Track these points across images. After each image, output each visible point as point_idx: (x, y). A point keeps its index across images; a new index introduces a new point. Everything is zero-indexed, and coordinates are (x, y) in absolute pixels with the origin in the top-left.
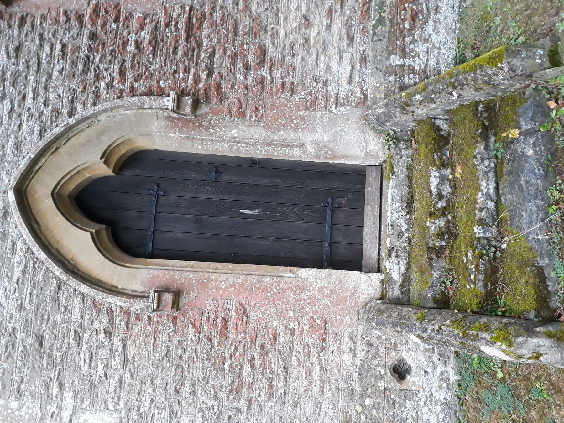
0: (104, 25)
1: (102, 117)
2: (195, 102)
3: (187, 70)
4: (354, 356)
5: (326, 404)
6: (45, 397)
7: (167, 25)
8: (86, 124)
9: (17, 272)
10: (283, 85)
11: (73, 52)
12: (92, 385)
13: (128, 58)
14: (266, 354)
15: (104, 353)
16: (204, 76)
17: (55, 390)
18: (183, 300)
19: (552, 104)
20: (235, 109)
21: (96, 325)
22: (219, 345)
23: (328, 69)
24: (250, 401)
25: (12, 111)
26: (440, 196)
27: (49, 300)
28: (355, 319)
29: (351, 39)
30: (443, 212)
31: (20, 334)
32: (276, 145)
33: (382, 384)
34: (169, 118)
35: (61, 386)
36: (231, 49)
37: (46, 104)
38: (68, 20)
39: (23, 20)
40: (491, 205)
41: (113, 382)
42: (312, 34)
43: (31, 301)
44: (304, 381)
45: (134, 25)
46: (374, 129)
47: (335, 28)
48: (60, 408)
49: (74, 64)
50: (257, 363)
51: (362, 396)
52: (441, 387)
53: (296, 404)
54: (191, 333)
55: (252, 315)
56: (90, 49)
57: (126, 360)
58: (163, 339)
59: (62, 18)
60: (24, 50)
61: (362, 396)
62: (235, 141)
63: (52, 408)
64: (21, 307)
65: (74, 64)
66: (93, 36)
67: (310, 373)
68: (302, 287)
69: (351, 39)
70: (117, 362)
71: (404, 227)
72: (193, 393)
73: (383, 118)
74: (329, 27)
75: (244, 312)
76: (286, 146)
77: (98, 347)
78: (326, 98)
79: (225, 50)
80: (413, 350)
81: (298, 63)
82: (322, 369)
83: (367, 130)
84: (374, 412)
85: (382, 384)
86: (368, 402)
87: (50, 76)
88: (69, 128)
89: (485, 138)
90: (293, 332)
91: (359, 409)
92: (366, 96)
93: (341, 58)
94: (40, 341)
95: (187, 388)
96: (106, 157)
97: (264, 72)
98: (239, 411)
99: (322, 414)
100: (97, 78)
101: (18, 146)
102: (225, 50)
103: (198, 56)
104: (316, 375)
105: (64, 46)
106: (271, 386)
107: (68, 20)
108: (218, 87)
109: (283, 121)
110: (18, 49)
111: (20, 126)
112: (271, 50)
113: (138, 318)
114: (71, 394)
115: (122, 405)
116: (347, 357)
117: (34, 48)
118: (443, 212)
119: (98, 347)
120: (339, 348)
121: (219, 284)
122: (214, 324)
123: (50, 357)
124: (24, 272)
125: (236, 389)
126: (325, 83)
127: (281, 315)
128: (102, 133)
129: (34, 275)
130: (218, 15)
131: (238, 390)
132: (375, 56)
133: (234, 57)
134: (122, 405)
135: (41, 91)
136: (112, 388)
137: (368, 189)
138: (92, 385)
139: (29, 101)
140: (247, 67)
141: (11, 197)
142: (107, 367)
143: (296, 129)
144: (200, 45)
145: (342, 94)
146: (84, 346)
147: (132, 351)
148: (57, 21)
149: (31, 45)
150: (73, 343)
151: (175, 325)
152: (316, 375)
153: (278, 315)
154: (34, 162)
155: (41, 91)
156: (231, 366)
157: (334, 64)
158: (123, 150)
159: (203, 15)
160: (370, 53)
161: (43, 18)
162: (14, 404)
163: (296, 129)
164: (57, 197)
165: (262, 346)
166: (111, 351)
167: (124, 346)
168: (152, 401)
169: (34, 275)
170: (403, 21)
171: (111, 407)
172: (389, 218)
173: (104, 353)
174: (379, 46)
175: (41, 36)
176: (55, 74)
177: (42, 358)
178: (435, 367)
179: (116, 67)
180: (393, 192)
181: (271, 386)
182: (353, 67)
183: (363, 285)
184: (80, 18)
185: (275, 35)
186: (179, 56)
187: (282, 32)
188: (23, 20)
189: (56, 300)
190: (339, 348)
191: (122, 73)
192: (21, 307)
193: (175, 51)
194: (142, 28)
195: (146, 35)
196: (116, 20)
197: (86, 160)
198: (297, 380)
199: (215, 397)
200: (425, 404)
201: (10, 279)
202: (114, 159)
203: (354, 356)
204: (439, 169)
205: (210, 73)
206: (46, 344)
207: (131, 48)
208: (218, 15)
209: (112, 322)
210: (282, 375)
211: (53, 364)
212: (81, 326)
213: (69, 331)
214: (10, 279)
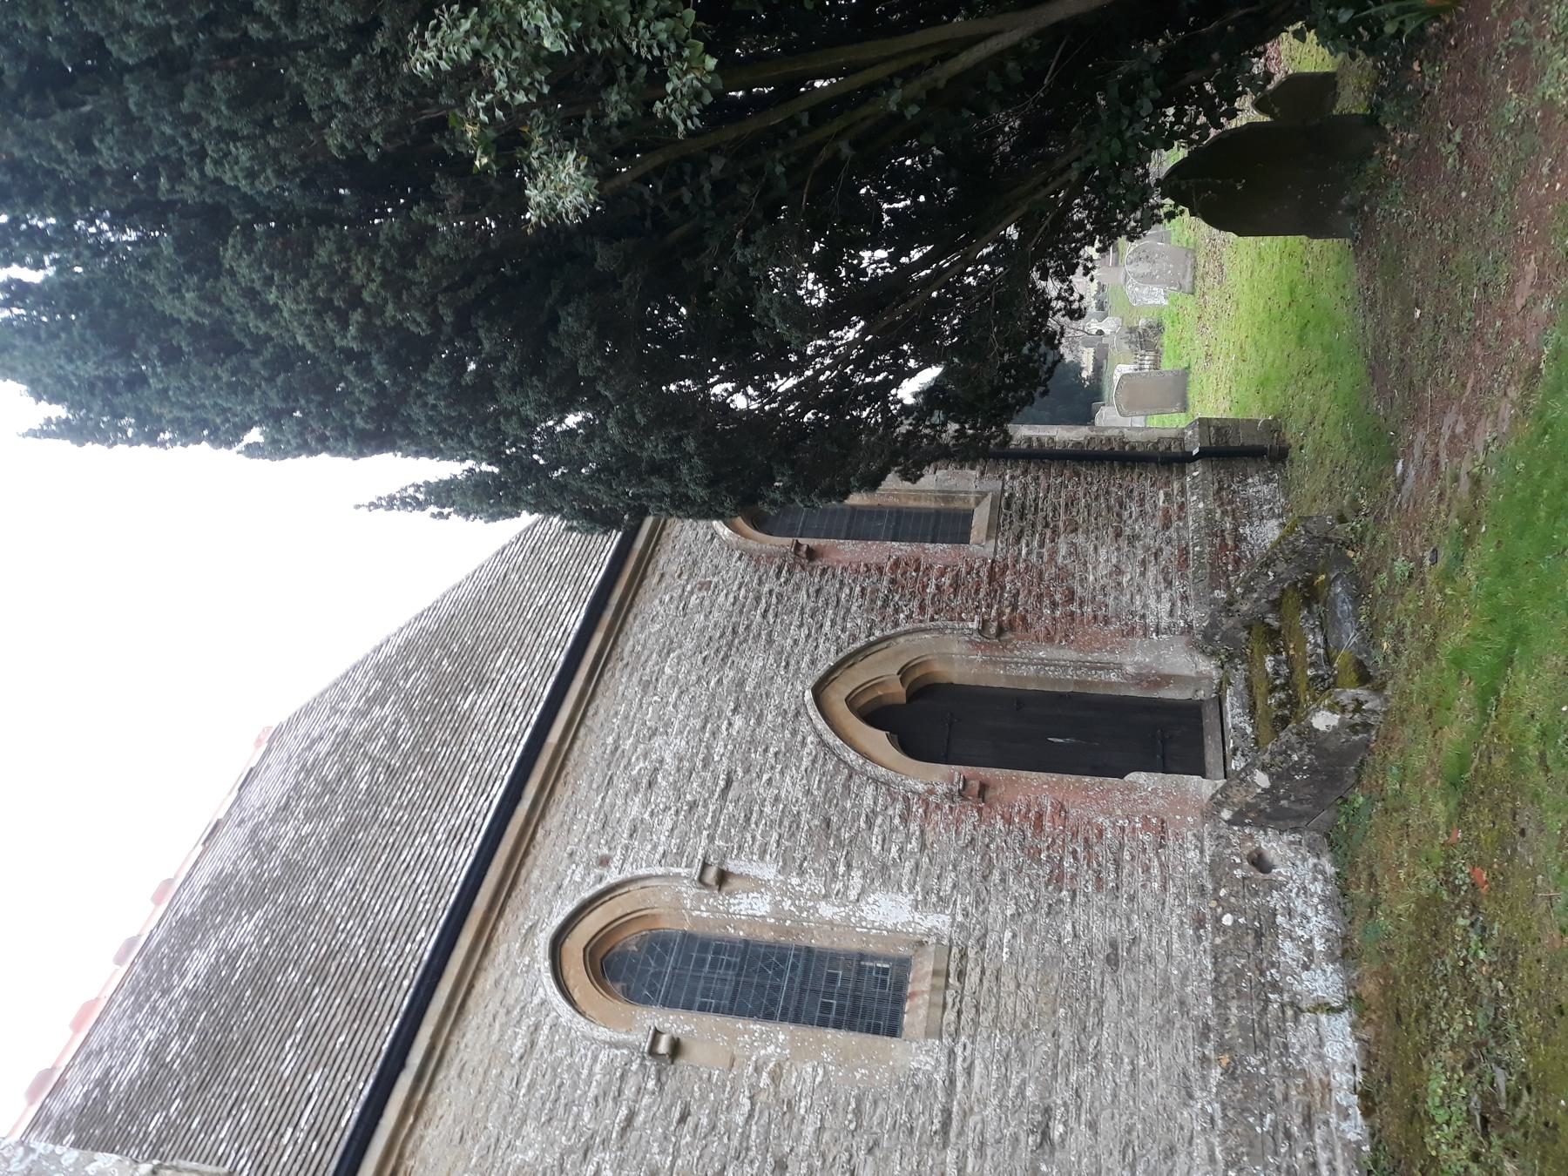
0: (904, 574)
1: (901, 640)
2: (1000, 632)
3: (989, 606)
4: (1202, 852)
5: (1170, 900)
6: (830, 875)
7: (968, 573)
8: (884, 645)
9: (806, 763)
10: (1095, 617)
11: (872, 592)
12: (884, 867)
13: (928, 598)
14: (1091, 847)
15: (898, 838)
16: (1008, 611)
17: (842, 869)
18: (989, 794)
19: (1351, 554)
20: (1041, 636)
21: (890, 812)
22: (1033, 835)
23: (1145, 606)
24: (1074, 892)
25: (809, 636)
26: (1277, 673)
27: (839, 788)
28: (1199, 819)
29: (1169, 584)
30: (1283, 687)
31: (805, 817)
32: (1091, 669)
33: (1238, 873)
34: (971, 642)
35: (849, 866)
36: (1035, 591)
37: (844, 630)
38: (869, 570)
39: (824, 571)
40: (1321, 651)
41: (909, 865)
42: (1125, 580)
43: (819, 788)
44: (1140, 876)
45: (934, 573)
46: (1203, 652)
47: (1150, 575)
48: (847, 887)
49: (873, 601)
50: (1081, 855)
51: (1216, 890)
52: (1315, 879)
53: (1132, 898)
54: (1000, 824)
55: (1073, 812)
56: (890, 591)
57: (923, 847)
58: (966, 828)
59: (862, 569)
60: (824, 592)
61: (1216, 890)
62: (1043, 663)
63: (839, 886)
64: (808, 792)
65: (873, 601)
66: (893, 581)
67: (1147, 869)
68: (1132, 788)
69: (1169, 584)
70: (913, 845)
71: (1249, 730)
72: (1003, 880)
73: (1210, 631)
74: (1143, 574)
75: (1060, 808)
76: (1101, 669)
77: (892, 831)
78: (1146, 628)
79: (1030, 592)
80: (1273, 845)
81: (1110, 601)
82: (1161, 865)
83: (1195, 653)
84: (1233, 900)
85: (1238, 873)
86: (1222, 892)
87: (848, 610)
88: (870, 645)
89: (1309, 606)
90: (1123, 829)
91: (1213, 904)
92: (1191, 627)
93: (1159, 597)
94: (828, 822)
95: (996, 877)
96: (904, 672)
97: (1074, 607)
98: (1061, 901)
99: (1167, 911)
100: (897, 611)
101: (813, 662)
102: (1030, 592)
103: (1001, 596)
104: (1155, 871)
105: (863, 589)
106: (1099, 879)
107: (869, 570)
108: (1024, 619)
109: (1097, 645)
110: (818, 591)
111: (817, 647)
112: (1079, 591)
113: (938, 806)
114: (860, 873)
115: (918, 888)
116: (1193, 855)
117: (833, 591)
118: (1283, 687)
119: (892, 831)
120: (1181, 846)
121: (1034, 788)
122: (1026, 816)
123: (837, 837)
124: (814, 762)
125: (1057, 879)
126: (1143, 616)
127: (1108, 813)
128: (898, 654)
129: (824, 765)
130: (1021, 566)
131: (1060, 879)
132: (1197, 594)
133: (1040, 597)
134: (918, 888)
135: (839, 621)
136: (907, 870)
137: (1206, 721)
138: (884, 867)
139: (827, 628)
140: (1054, 605)
141: (808, 695)
142: (901, 850)
143: (1112, 651)
144: (1003, 588)
145: (1163, 625)
146: (876, 830)
147: (930, 837)
148: (857, 571)
149: (831, 588)
150: (863, 825)
151: (980, 815)
152: (1155, 871)
153: (1102, 812)
154: (832, 671)
155: (839, 621)
156: (1048, 856)
157: (1152, 602)
158: (918, 673)
159: (1006, 566)
160: (1191, 593)
161: (845, 569)
162: (795, 881)
163: (1112, 651)
164: (850, 701)
165: (1086, 840)
166: (907, 835)
167: (922, 832)
168: (954, 886)
169: (824, 765)
170: (1226, 564)
171: (905, 889)
172: (1229, 721)
173: (898, 838)
174: (1201, 586)
175: (841, 582)
176: (854, 608)
177: (828, 838)
178: (1304, 860)
179: (916, 603)
180: (1234, 715)
181: (1099, 879)
182: (1173, 604)
183: (1203, 788)
184: (880, 569)
185: (1083, 580)
186: (981, 595)
187: (1091, 578)
188: (824, 571)
189: (846, 787)
190: (1181, 846)
191: (922, 608)
192: (808, 792)
193: (977, 592)
194: (942, 575)
195: (946, 580)
196: (917, 570)
197: (883, 674)
198: (1131, 875)
199: (1031, 885)
200: (1297, 895)
201: (798, 769)
202: (909, 680)
203: (1202, 852)
204: (1272, 654)
205: (1014, 608)
206: (834, 826)
207: (931, 589)
208: (1021, 566)
209: (908, 808)
210: (1112, 868)
211: (840, 843)
212: (873, 811)
213: (859, 815)
214: (798, 769)
